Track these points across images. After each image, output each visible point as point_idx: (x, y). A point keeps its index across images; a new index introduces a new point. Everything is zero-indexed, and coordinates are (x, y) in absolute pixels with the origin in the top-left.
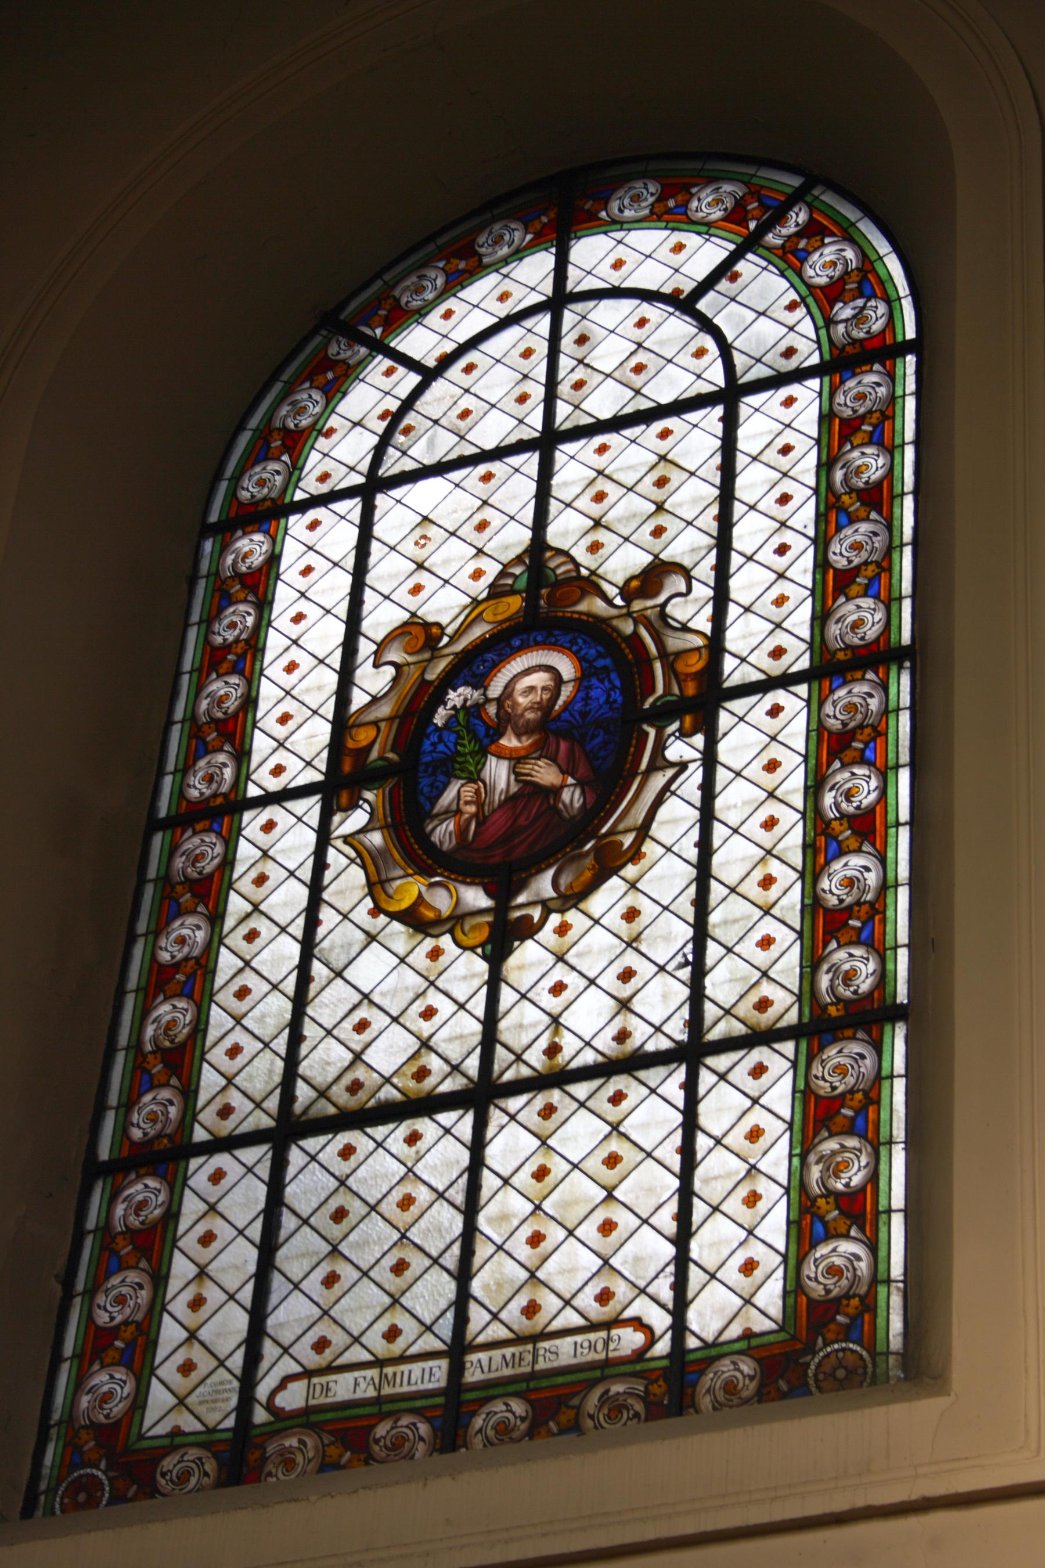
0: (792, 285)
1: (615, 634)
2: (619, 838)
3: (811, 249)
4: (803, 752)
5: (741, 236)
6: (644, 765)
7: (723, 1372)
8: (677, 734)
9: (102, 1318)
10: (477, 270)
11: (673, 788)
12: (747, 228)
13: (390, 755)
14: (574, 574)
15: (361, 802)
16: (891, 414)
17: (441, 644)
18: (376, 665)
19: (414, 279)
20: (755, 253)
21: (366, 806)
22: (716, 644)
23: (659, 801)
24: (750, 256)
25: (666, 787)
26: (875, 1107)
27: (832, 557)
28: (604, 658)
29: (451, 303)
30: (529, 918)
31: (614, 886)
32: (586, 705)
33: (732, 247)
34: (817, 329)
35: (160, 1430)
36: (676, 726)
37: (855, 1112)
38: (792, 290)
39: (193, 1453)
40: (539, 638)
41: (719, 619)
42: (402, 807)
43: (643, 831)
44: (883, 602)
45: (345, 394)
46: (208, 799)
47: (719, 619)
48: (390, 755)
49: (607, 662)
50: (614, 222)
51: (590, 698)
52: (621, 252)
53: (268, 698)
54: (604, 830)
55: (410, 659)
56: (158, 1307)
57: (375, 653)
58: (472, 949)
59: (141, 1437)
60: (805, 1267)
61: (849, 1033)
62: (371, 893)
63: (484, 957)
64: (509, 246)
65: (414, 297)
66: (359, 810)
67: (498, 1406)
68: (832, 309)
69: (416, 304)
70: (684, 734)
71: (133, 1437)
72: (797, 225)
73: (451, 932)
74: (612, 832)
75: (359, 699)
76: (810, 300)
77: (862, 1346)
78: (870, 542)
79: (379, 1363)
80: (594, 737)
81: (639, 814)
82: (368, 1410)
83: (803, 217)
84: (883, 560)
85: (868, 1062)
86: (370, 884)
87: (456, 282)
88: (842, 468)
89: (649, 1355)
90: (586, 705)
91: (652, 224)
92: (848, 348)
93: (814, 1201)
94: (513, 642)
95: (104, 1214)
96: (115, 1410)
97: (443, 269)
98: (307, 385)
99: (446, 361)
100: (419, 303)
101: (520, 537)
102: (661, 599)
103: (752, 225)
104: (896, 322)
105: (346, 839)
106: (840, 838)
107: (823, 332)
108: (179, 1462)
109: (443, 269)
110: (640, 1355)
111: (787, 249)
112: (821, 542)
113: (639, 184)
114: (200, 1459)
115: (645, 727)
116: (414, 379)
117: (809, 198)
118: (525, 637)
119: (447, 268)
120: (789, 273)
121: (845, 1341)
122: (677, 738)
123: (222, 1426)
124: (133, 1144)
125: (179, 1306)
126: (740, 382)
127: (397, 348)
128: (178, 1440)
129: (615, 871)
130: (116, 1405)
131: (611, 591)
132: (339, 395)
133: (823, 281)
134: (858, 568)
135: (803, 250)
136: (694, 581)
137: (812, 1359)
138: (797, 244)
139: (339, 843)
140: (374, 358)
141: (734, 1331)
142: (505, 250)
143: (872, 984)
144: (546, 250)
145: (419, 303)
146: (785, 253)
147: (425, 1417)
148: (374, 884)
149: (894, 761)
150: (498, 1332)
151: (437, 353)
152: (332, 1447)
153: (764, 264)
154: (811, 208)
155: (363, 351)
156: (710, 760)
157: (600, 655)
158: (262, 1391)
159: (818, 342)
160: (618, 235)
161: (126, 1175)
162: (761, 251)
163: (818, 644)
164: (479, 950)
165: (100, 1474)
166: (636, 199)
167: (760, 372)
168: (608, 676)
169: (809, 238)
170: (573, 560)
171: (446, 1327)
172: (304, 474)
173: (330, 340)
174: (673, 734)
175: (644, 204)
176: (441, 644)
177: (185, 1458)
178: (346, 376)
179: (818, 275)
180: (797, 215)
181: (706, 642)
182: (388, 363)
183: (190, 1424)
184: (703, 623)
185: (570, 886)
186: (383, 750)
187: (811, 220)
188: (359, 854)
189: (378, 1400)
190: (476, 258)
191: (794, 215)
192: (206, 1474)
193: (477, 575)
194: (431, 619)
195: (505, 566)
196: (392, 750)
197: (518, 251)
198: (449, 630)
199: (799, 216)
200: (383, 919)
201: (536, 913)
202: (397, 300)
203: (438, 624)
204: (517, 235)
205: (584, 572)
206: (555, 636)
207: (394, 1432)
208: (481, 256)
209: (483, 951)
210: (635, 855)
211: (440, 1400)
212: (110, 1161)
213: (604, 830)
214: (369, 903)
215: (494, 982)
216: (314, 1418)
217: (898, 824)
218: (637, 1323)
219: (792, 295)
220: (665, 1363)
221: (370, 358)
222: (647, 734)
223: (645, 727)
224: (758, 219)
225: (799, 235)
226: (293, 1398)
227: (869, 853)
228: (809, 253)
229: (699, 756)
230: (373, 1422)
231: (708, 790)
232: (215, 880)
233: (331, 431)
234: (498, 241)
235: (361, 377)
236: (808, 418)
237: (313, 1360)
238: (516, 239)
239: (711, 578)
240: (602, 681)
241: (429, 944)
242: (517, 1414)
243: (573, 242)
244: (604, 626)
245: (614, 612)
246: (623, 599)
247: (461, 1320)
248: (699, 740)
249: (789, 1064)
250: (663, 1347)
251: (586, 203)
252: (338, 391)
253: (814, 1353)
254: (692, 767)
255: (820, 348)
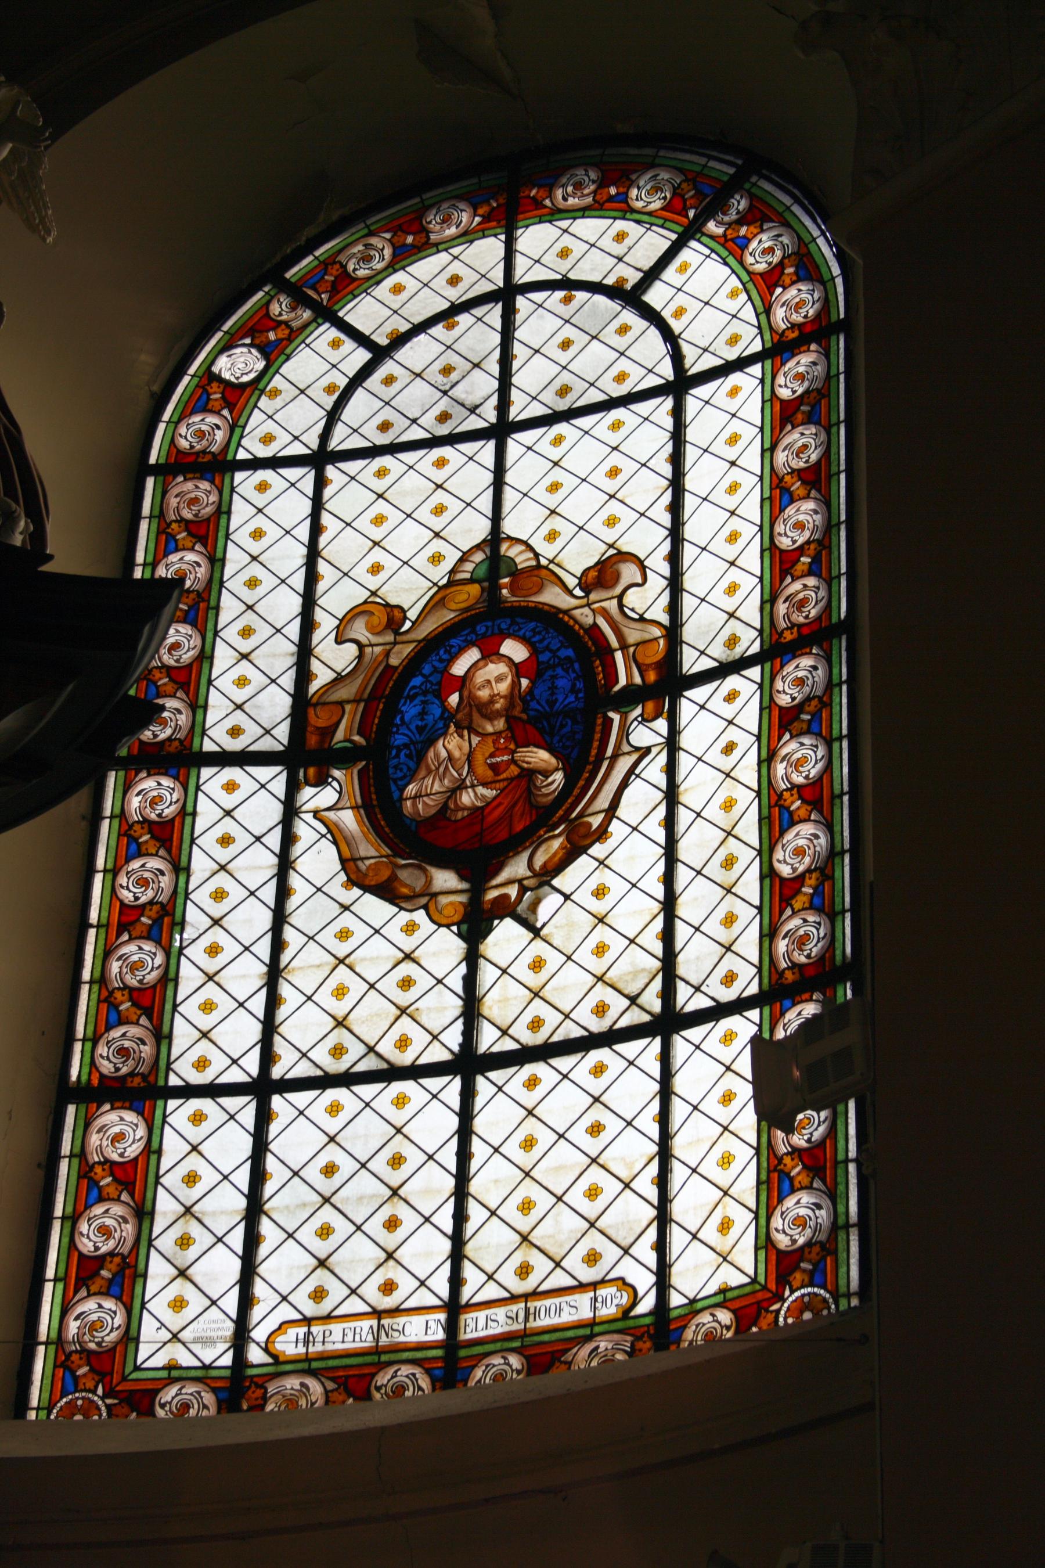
0: (733, 271)
1: (577, 627)
2: (590, 819)
3: (750, 236)
4: (758, 627)
5: (681, 225)
6: (609, 752)
7: (704, 1324)
8: (640, 719)
9: (86, 1246)
10: (425, 247)
11: (637, 772)
12: (687, 216)
13: (356, 738)
14: (534, 563)
15: (330, 780)
16: (830, 873)
17: (403, 629)
18: (339, 641)
19: (360, 247)
20: (699, 241)
21: (335, 784)
22: (673, 631)
23: (624, 784)
24: (693, 244)
25: (631, 771)
26: (830, 882)
27: (776, 865)
28: (566, 647)
29: (399, 277)
30: (506, 897)
31: (583, 864)
32: (552, 694)
33: (674, 237)
34: (757, 315)
35: (158, 1361)
36: (638, 711)
37: (813, 1265)
38: (281, 371)
39: (191, 1389)
40: (503, 626)
41: (674, 608)
42: (376, 721)
43: (611, 812)
44: (824, 580)
45: (288, 358)
46: (197, 454)
47: (674, 608)
48: (356, 738)
49: (570, 652)
50: (560, 211)
51: (556, 688)
52: (567, 241)
53: (165, 1213)
54: (574, 815)
55: (375, 640)
56: (143, 1240)
57: (338, 627)
58: (448, 926)
59: (137, 1368)
60: (776, 525)
61: (805, 996)
62: (344, 868)
63: (459, 935)
64: (457, 227)
65: (362, 265)
66: (329, 787)
67: (497, 1360)
68: (771, 295)
69: (362, 273)
70: (645, 720)
71: (129, 1367)
72: (738, 213)
73: (426, 907)
74: (581, 815)
75: (321, 676)
76: (750, 286)
77: (826, 1290)
78: (811, 846)
79: (377, 1313)
80: (562, 726)
81: (603, 801)
82: (368, 1359)
83: (743, 204)
84: (824, 694)
85: (820, 672)
86: (343, 861)
87: (402, 257)
88: (785, 602)
89: (633, 1314)
90: (552, 694)
91: (597, 213)
92: (787, 333)
93: (780, 1160)
94: (478, 628)
95: (98, 969)
96: (184, 656)
97: (389, 240)
98: (248, 341)
99: (400, 340)
100: (367, 272)
101: (481, 528)
102: (618, 590)
103: (691, 214)
104: (832, 309)
105: (316, 814)
106: (792, 1174)
107: (763, 318)
108: (177, 1395)
109: (389, 240)
110: (626, 1313)
111: (729, 237)
112: (766, 851)
113: (580, 172)
114: (199, 1393)
115: (611, 714)
116: (363, 356)
117: (747, 186)
118: (489, 624)
119: (394, 241)
120: (731, 260)
121: (812, 1285)
122: (640, 723)
123: (217, 1364)
124: (179, 452)
125: (166, 1242)
126: (690, 373)
127: (346, 318)
128: (175, 1373)
129: (583, 850)
130: (149, 973)
131: (571, 582)
132: (283, 357)
133: (761, 267)
134: (802, 877)
135: (744, 237)
136: (648, 570)
137: (782, 1305)
138: (738, 231)
139: (309, 817)
140: (319, 325)
141: (711, 1288)
142: (453, 231)
143: (822, 947)
144: (495, 236)
145: (367, 272)
146: (726, 241)
147: (424, 1368)
148: (348, 860)
149: (841, 907)
150: (492, 1292)
151: (388, 328)
152: (335, 1394)
153: (707, 252)
154: (752, 197)
155: (307, 315)
156: (672, 744)
157: (563, 646)
158: (259, 1334)
159: (759, 327)
160: (564, 224)
161: (174, 478)
162: (704, 239)
163: (767, 963)
164: (455, 928)
165: (96, 1398)
166: (578, 186)
167: (708, 362)
168: (572, 666)
169: (748, 224)
170: (530, 548)
171: (441, 1285)
172: (247, 430)
173: (272, 297)
174: (636, 719)
175: (586, 191)
176: (403, 629)
177: (183, 1391)
178: (290, 339)
179: (757, 262)
180: (739, 202)
181: (664, 632)
182: (334, 333)
183: (186, 1359)
184: (659, 613)
185: (545, 865)
186: (349, 729)
187: (751, 208)
188: (330, 831)
189: (377, 1350)
190: (424, 235)
191: (736, 203)
192: (205, 1407)
193: (436, 559)
194: (393, 601)
195: (464, 553)
196: (359, 733)
197: (465, 234)
198: (412, 614)
199: (740, 204)
200: (356, 892)
201: (513, 891)
202: (344, 267)
203: (399, 607)
204: (465, 217)
205: (543, 562)
206: (518, 624)
207: (395, 1380)
208: (427, 232)
209: (458, 929)
210: (602, 834)
211: (439, 1353)
212: (157, 464)
213: (574, 815)
214: (343, 877)
215: (472, 959)
216: (315, 1365)
217: (847, 1161)
218: (622, 1283)
219: (734, 282)
220: (647, 1321)
221: (314, 325)
222: (612, 720)
223: (611, 714)
224: (696, 208)
225: (741, 221)
226: (289, 1345)
227: (820, 1190)
228: (749, 240)
229: (664, 740)
230: (374, 1371)
231: (671, 769)
232: (176, 824)
233: (275, 393)
234: (446, 221)
235: (308, 341)
236: (753, 409)
237: (310, 1309)
238: (464, 220)
239: (665, 569)
240: (566, 671)
241: (404, 917)
242: (514, 1367)
243: (519, 232)
244: (566, 618)
245: (575, 602)
246: (581, 589)
247: (456, 1281)
248: (661, 725)
249: (757, 633)
250: (647, 1304)
251: (530, 191)
252: (282, 353)
253: (784, 1300)
254: (654, 751)
255: (761, 333)
